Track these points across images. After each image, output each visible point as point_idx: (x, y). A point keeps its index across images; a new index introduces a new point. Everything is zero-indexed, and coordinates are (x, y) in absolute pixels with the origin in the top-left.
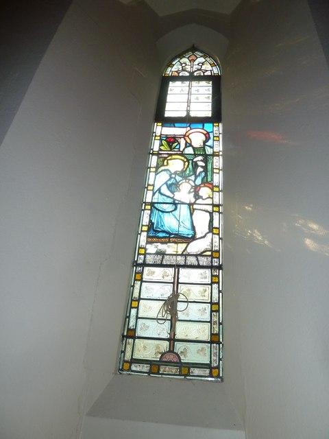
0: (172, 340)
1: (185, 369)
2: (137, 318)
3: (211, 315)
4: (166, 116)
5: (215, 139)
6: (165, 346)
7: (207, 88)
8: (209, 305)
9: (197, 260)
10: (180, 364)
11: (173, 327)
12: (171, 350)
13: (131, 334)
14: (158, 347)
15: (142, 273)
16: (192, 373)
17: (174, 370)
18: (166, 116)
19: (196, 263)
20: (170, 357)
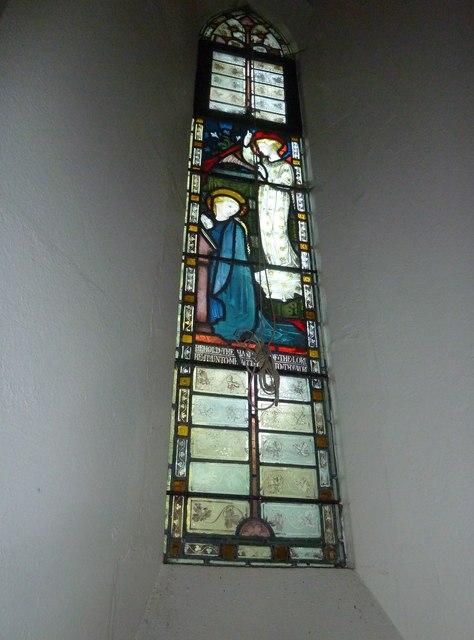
0: (255, 498)
1: (282, 551)
2: (316, 468)
3: (316, 455)
4: (212, 106)
5: (196, 144)
6: (242, 508)
7: (277, 102)
8: (312, 438)
9: (237, 355)
10: (270, 540)
11: (254, 476)
12: (255, 516)
13: (180, 491)
14: (229, 511)
15: (190, 375)
16: (243, 554)
17: (265, 552)
18: (212, 106)
19: (234, 361)
20: (255, 530)
